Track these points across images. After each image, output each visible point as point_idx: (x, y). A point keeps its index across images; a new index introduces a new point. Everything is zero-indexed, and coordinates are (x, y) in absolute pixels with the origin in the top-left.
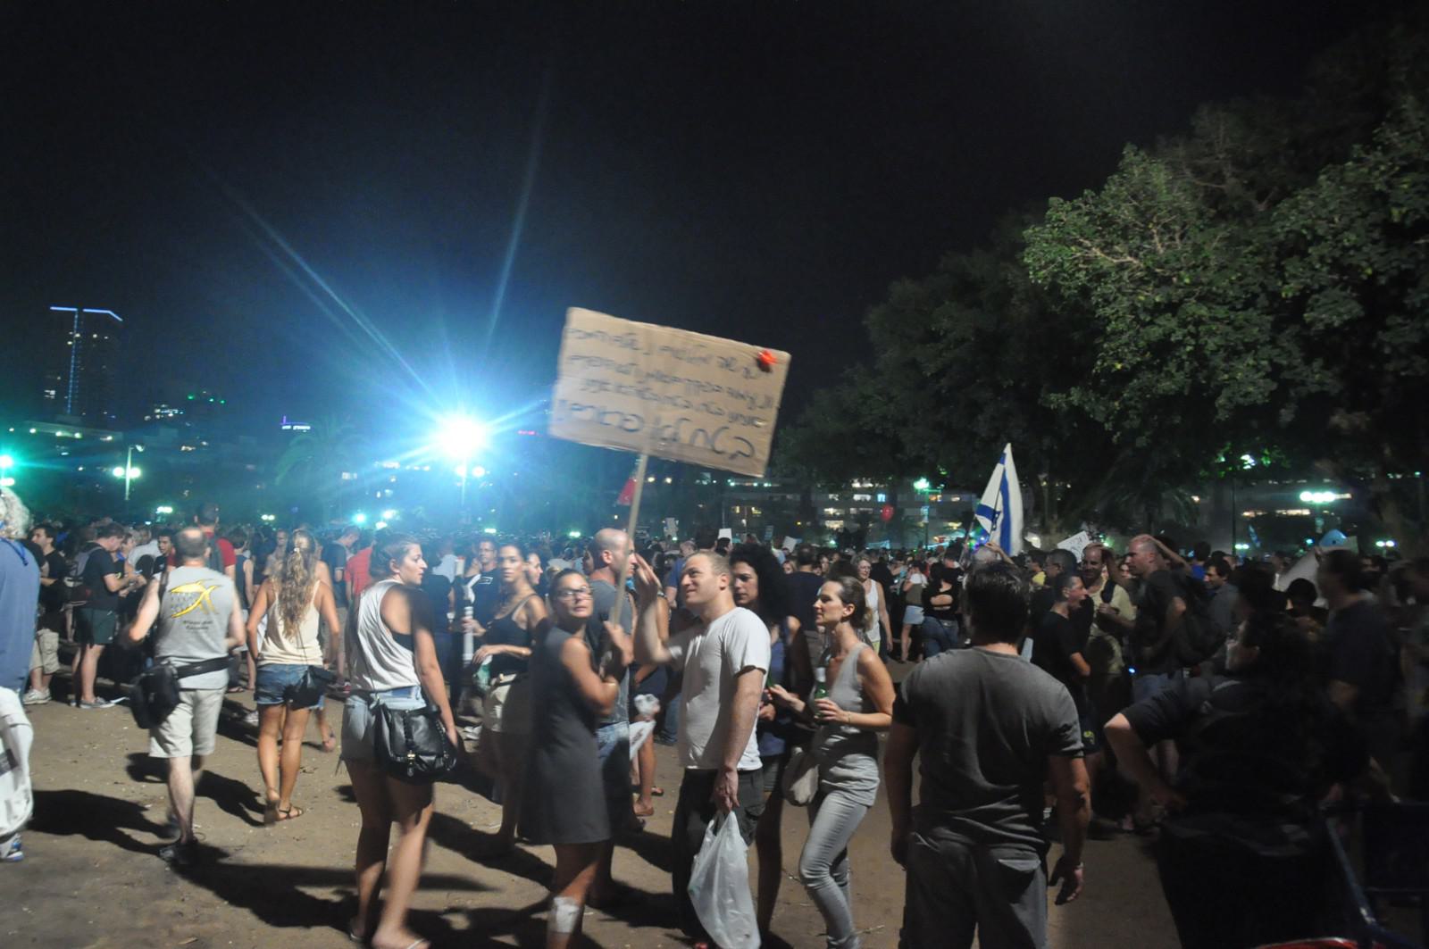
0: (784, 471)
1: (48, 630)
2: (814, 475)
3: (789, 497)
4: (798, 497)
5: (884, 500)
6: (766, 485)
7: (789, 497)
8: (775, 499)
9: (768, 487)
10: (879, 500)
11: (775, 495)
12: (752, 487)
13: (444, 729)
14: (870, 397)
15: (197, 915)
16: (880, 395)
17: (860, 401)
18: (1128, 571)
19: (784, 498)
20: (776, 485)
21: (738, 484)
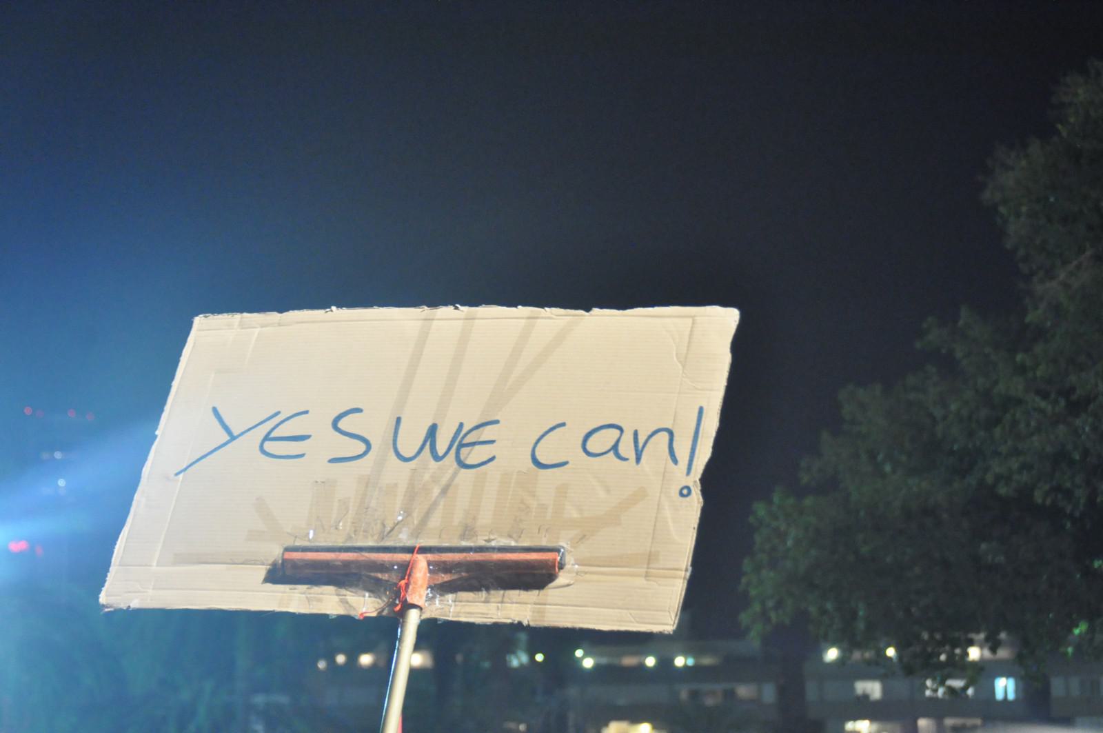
0: (773, 615)
1: (357, 618)
2: (861, 625)
3: (744, 691)
4: (769, 693)
5: (1011, 696)
6: (680, 661)
7: (744, 691)
8: (710, 702)
9: (686, 667)
10: (999, 695)
11: (706, 687)
12: (642, 666)
13: (544, 571)
14: (1011, 402)
15: (500, 605)
16: (1045, 395)
17: (984, 413)
18: (927, 688)
19: (730, 694)
20: (707, 661)
21: (604, 660)
